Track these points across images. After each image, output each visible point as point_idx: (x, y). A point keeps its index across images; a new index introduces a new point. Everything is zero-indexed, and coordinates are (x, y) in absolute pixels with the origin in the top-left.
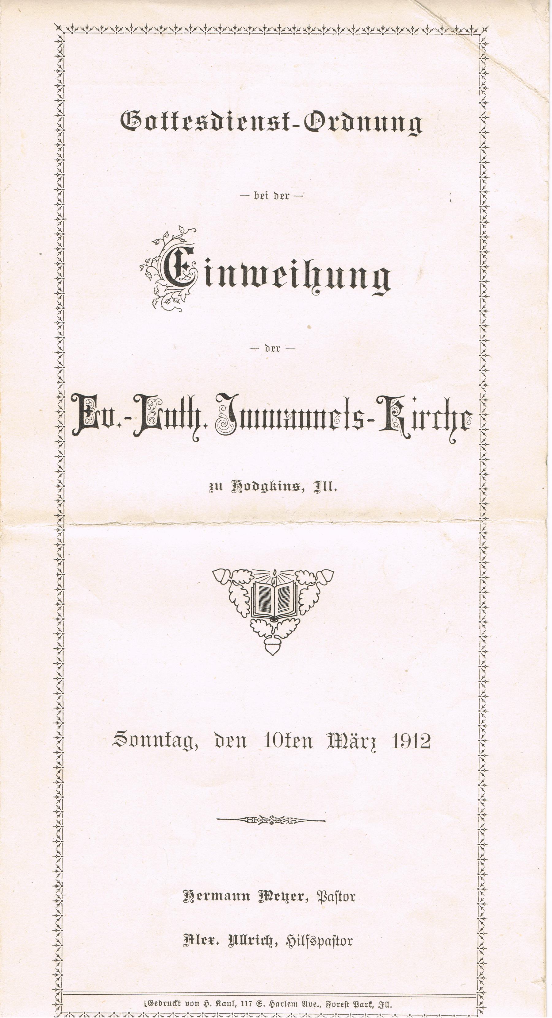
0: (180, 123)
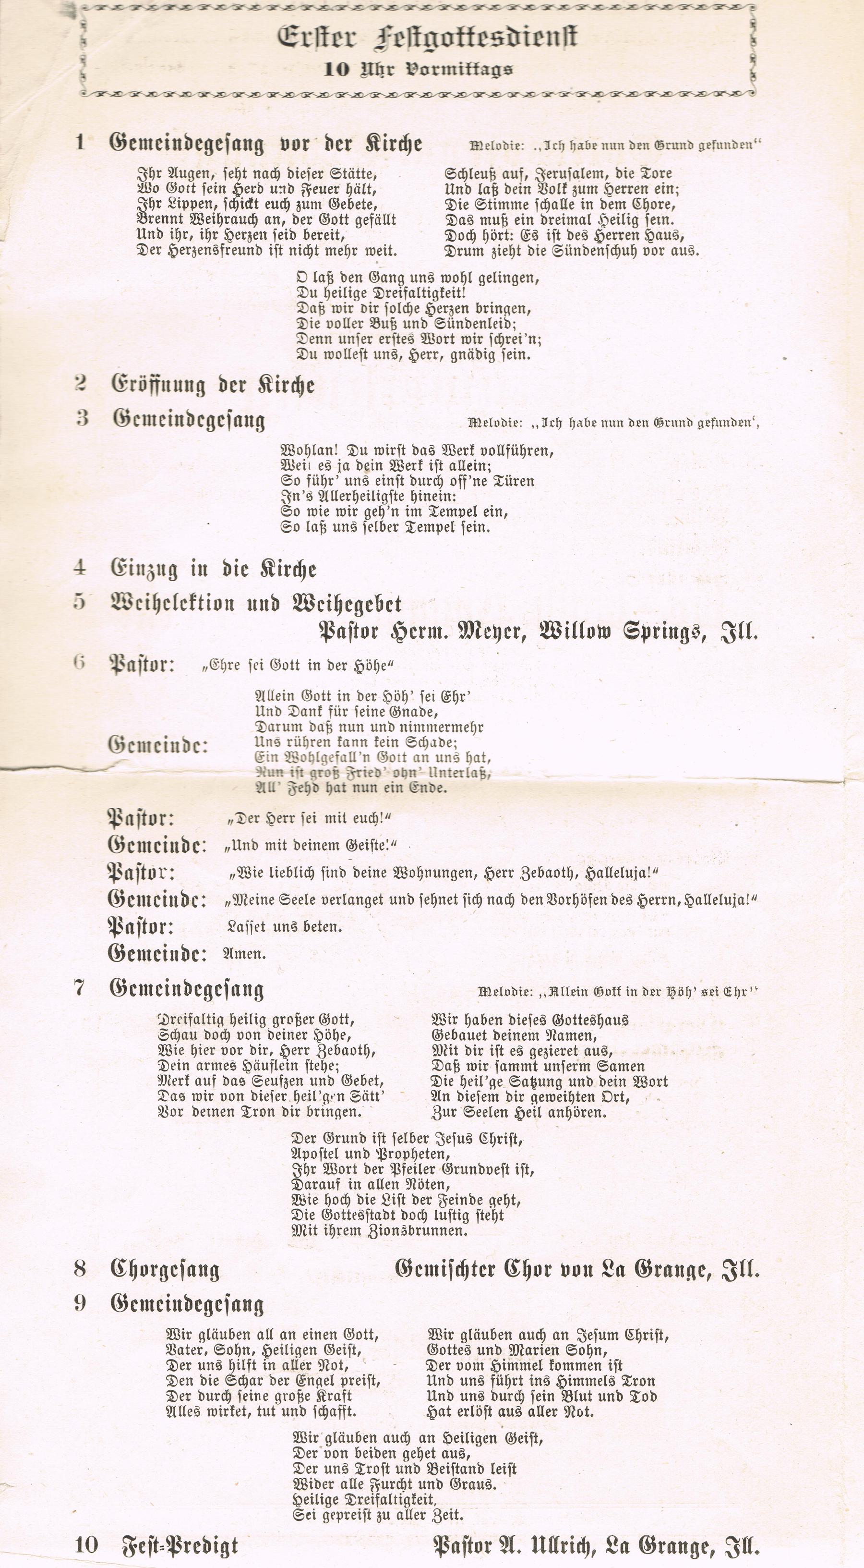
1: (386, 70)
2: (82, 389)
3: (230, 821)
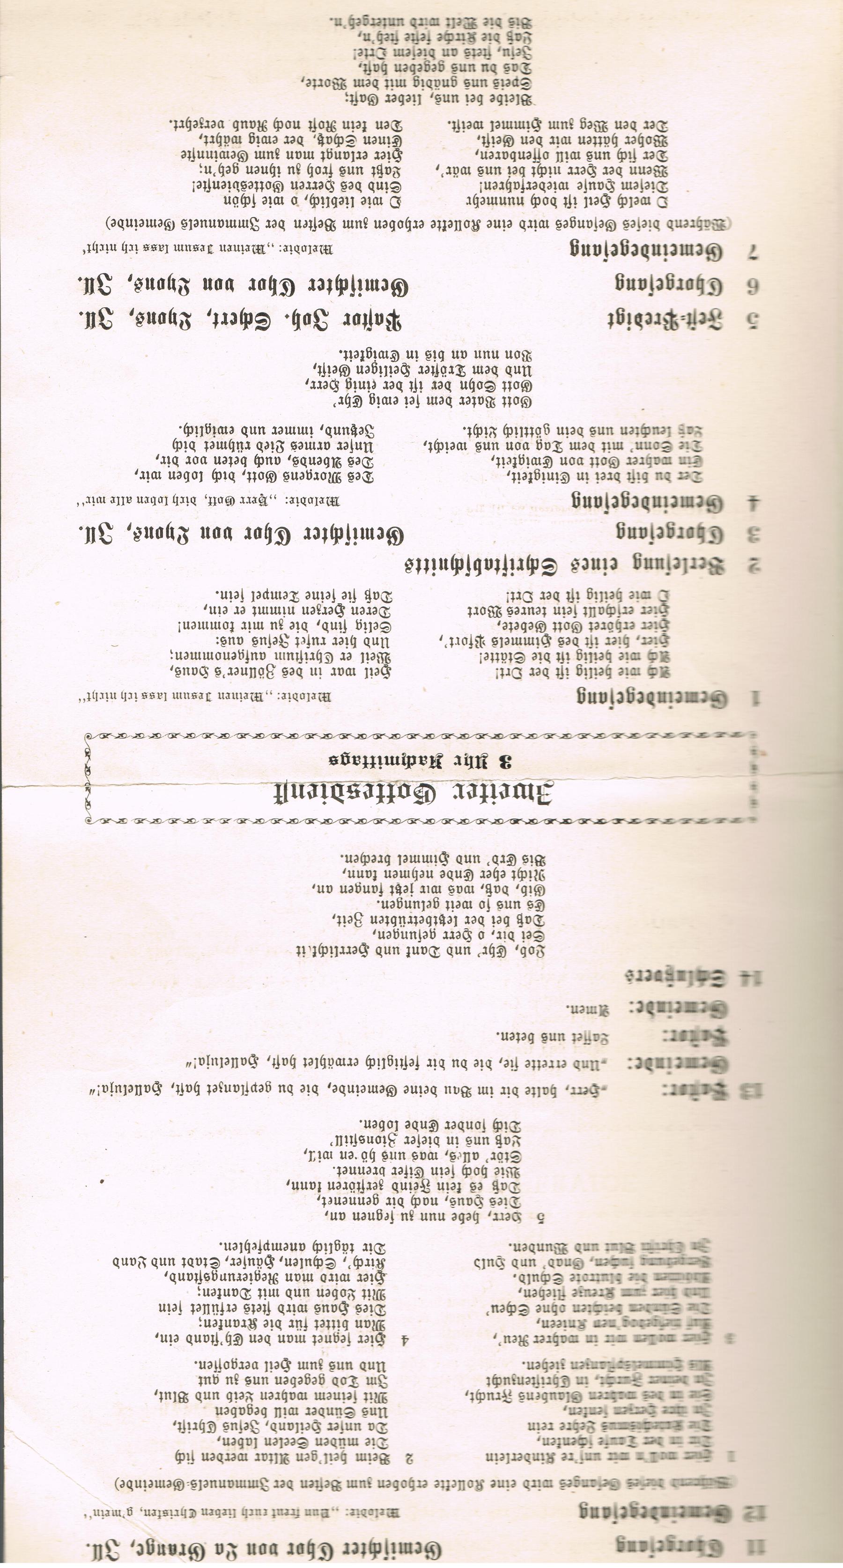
0: (376, 791)
1: (463, 761)
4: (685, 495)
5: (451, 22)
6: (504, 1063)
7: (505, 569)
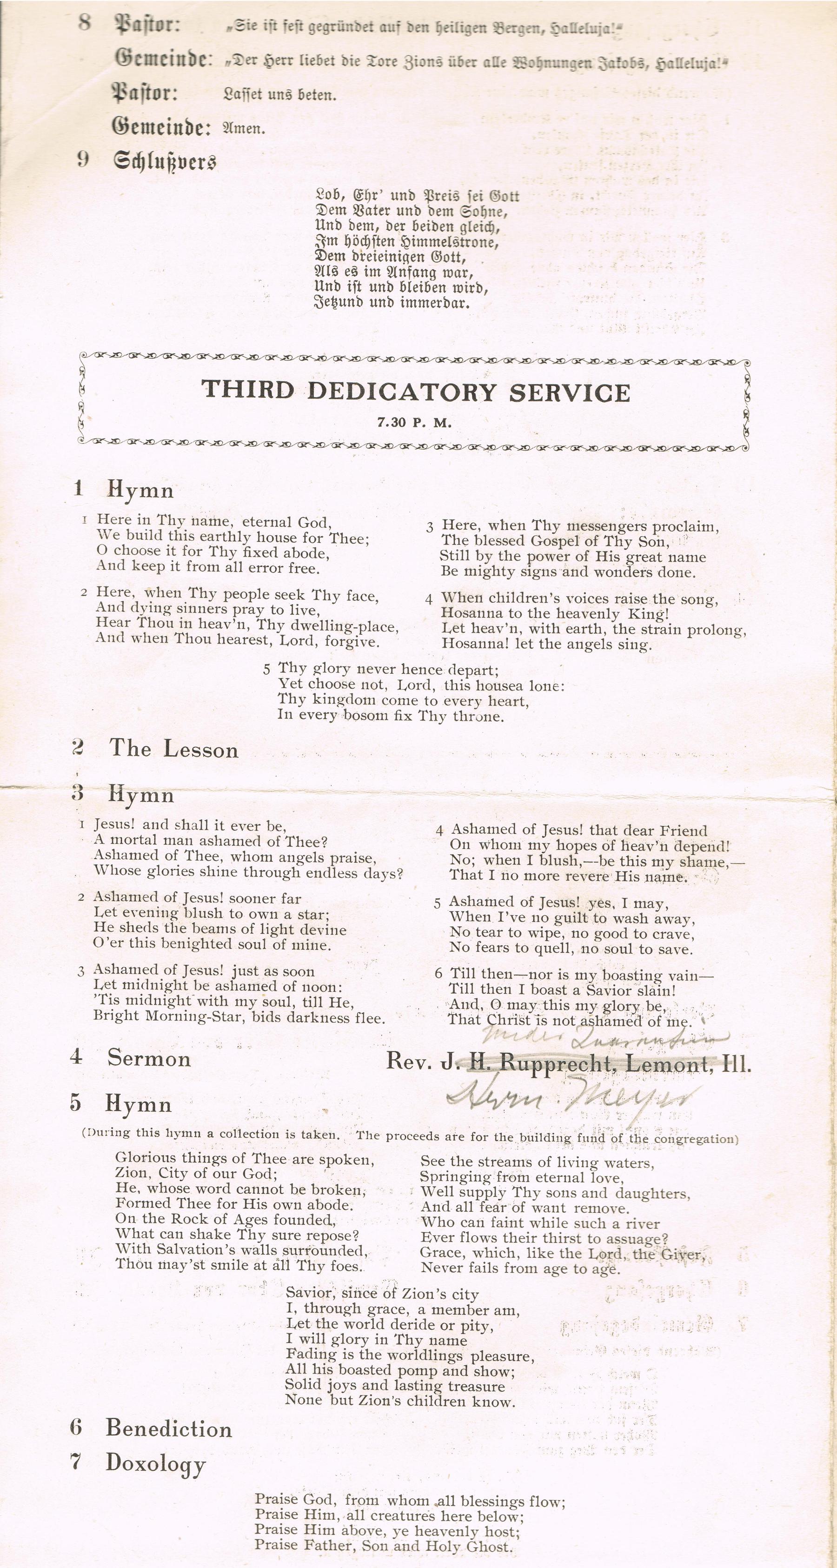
2: (80, 753)
3: (228, 63)
4: (153, 66)
5: (514, 197)
6: (503, 214)
7: (409, 270)
